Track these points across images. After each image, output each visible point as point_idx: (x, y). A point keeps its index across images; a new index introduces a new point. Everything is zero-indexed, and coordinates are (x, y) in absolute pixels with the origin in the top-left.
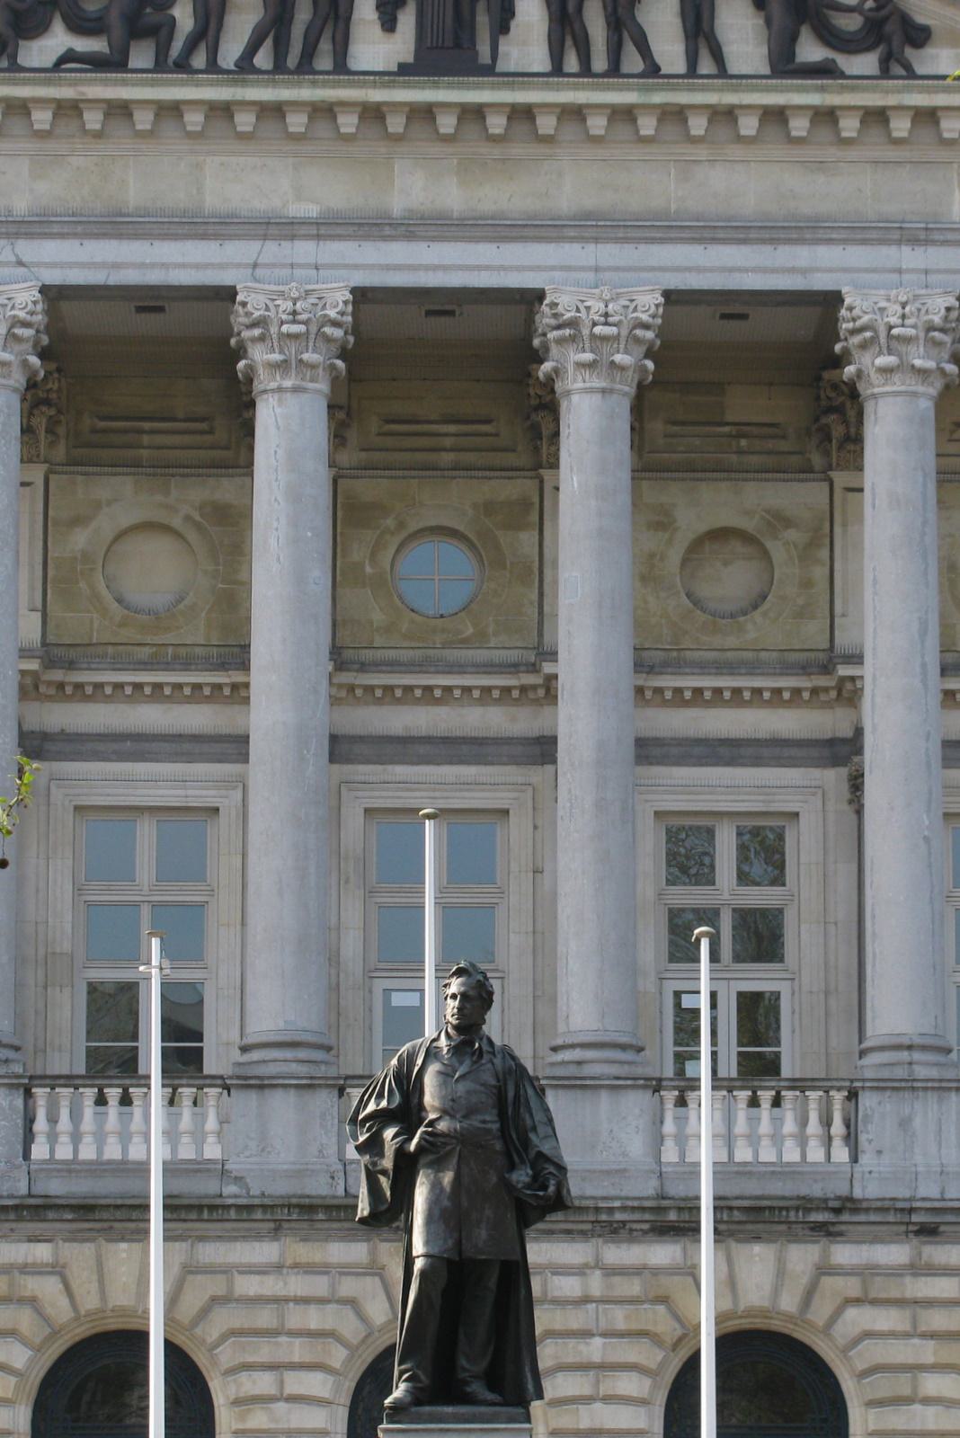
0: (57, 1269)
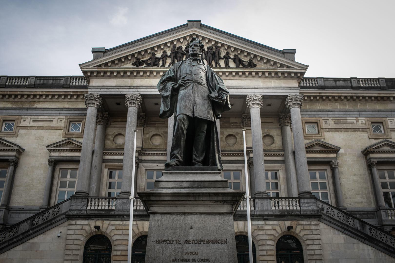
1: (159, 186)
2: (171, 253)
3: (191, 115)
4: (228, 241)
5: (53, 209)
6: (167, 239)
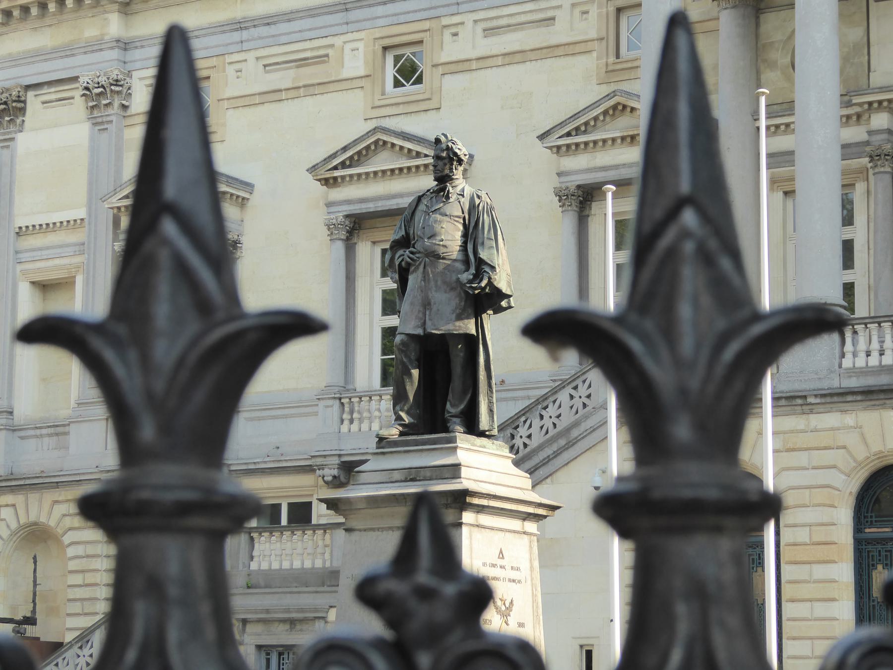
3: (420, 331)
5: (569, 390)
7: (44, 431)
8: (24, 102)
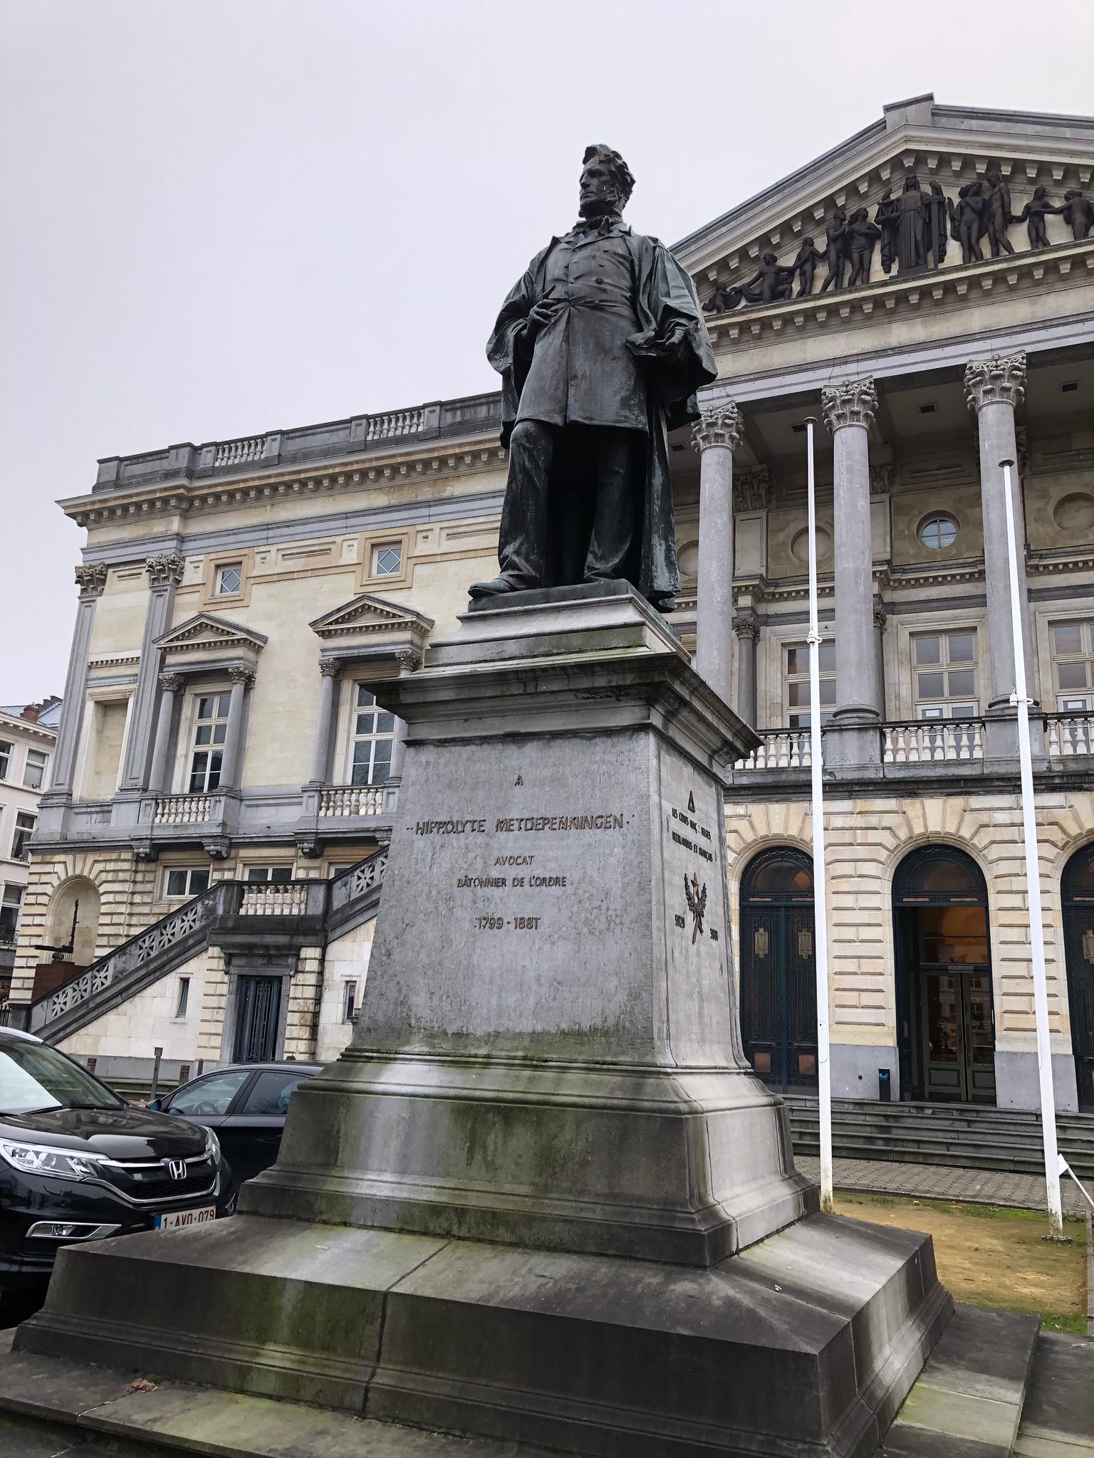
0: (747, 816)
1: (437, 659)
2: (457, 861)
3: (557, 420)
4: (625, 821)
6: (447, 820)
7: (93, 809)
8: (106, 576)
